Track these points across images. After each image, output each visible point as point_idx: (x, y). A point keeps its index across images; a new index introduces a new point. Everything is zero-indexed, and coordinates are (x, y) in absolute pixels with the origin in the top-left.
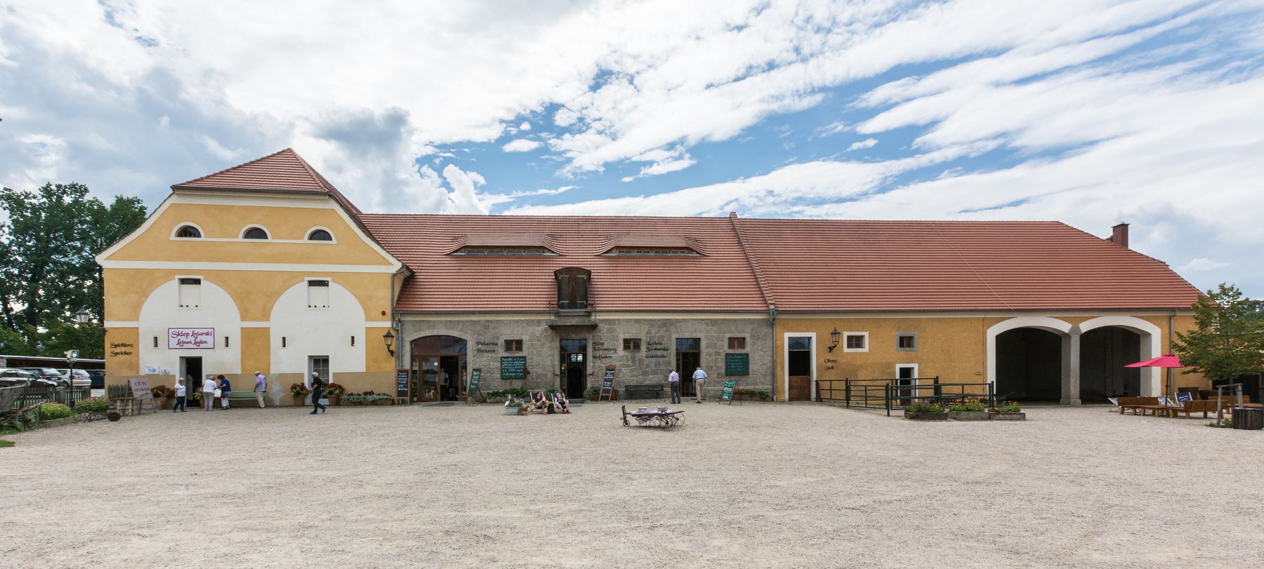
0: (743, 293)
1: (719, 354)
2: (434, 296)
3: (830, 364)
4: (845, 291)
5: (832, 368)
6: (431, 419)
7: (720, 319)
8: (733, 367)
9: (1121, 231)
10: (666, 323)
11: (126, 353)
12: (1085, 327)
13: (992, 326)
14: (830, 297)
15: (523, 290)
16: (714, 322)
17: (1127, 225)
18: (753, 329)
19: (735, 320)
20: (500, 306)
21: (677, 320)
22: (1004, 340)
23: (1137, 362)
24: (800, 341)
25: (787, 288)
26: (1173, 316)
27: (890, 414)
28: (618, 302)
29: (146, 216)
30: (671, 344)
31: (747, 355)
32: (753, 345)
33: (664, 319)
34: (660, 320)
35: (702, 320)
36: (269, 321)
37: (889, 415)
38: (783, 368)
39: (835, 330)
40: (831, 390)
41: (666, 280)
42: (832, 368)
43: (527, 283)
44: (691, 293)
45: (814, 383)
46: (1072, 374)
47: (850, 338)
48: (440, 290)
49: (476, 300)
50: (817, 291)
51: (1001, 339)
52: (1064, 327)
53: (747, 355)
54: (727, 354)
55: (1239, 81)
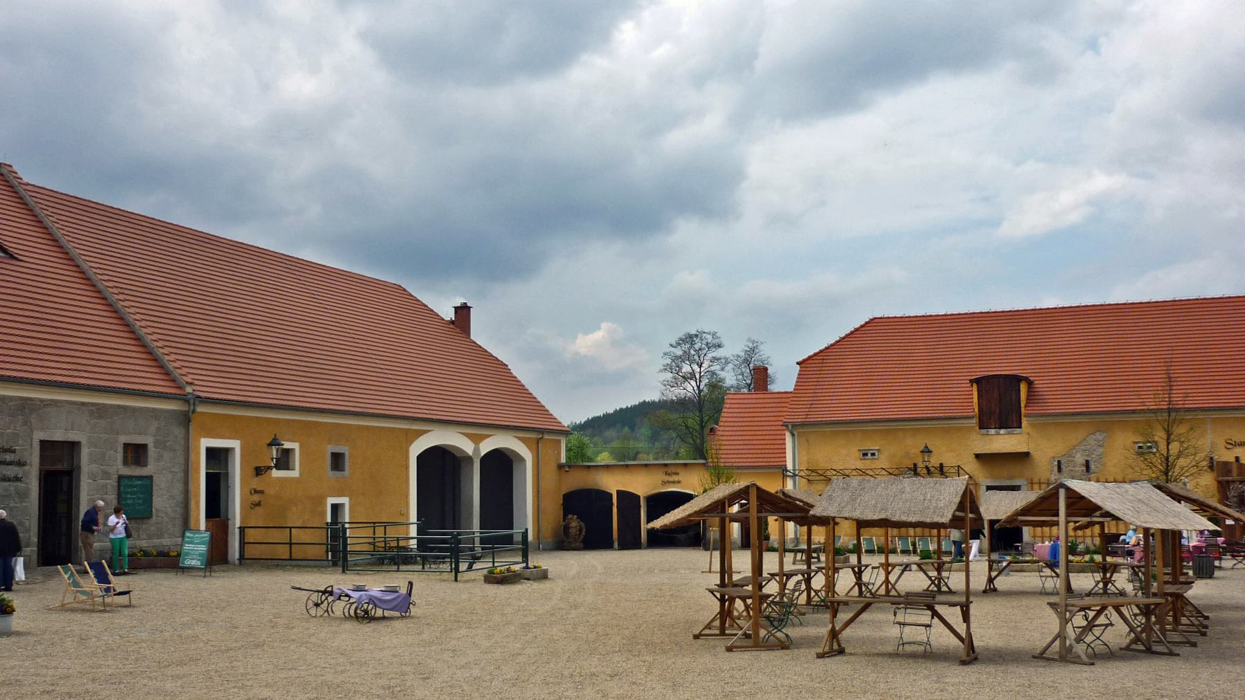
1: (106, 475)
3: (256, 498)
5: (258, 504)
7: (111, 406)
8: (129, 502)
9: (798, 363)
10: (26, 405)
11: (17, 479)
12: (486, 447)
13: (414, 441)
16: (101, 410)
17: (470, 307)
18: (158, 429)
19: (134, 410)
20: (951, 390)
21: (42, 401)
22: (145, 465)
23: (612, 497)
24: (507, 453)
26: (541, 438)
27: (459, 579)
28: (887, 396)
30: (31, 454)
31: (150, 478)
32: (159, 458)
33: (21, 398)
34: (12, 398)
35: (83, 404)
37: (456, 580)
38: (198, 502)
39: (275, 439)
40: (291, 544)
42: (258, 504)
44: (345, 361)
45: (237, 531)
46: (475, 513)
47: (227, 452)
49: (905, 369)
51: (421, 458)
52: (467, 447)
53: (150, 478)
54: (120, 478)
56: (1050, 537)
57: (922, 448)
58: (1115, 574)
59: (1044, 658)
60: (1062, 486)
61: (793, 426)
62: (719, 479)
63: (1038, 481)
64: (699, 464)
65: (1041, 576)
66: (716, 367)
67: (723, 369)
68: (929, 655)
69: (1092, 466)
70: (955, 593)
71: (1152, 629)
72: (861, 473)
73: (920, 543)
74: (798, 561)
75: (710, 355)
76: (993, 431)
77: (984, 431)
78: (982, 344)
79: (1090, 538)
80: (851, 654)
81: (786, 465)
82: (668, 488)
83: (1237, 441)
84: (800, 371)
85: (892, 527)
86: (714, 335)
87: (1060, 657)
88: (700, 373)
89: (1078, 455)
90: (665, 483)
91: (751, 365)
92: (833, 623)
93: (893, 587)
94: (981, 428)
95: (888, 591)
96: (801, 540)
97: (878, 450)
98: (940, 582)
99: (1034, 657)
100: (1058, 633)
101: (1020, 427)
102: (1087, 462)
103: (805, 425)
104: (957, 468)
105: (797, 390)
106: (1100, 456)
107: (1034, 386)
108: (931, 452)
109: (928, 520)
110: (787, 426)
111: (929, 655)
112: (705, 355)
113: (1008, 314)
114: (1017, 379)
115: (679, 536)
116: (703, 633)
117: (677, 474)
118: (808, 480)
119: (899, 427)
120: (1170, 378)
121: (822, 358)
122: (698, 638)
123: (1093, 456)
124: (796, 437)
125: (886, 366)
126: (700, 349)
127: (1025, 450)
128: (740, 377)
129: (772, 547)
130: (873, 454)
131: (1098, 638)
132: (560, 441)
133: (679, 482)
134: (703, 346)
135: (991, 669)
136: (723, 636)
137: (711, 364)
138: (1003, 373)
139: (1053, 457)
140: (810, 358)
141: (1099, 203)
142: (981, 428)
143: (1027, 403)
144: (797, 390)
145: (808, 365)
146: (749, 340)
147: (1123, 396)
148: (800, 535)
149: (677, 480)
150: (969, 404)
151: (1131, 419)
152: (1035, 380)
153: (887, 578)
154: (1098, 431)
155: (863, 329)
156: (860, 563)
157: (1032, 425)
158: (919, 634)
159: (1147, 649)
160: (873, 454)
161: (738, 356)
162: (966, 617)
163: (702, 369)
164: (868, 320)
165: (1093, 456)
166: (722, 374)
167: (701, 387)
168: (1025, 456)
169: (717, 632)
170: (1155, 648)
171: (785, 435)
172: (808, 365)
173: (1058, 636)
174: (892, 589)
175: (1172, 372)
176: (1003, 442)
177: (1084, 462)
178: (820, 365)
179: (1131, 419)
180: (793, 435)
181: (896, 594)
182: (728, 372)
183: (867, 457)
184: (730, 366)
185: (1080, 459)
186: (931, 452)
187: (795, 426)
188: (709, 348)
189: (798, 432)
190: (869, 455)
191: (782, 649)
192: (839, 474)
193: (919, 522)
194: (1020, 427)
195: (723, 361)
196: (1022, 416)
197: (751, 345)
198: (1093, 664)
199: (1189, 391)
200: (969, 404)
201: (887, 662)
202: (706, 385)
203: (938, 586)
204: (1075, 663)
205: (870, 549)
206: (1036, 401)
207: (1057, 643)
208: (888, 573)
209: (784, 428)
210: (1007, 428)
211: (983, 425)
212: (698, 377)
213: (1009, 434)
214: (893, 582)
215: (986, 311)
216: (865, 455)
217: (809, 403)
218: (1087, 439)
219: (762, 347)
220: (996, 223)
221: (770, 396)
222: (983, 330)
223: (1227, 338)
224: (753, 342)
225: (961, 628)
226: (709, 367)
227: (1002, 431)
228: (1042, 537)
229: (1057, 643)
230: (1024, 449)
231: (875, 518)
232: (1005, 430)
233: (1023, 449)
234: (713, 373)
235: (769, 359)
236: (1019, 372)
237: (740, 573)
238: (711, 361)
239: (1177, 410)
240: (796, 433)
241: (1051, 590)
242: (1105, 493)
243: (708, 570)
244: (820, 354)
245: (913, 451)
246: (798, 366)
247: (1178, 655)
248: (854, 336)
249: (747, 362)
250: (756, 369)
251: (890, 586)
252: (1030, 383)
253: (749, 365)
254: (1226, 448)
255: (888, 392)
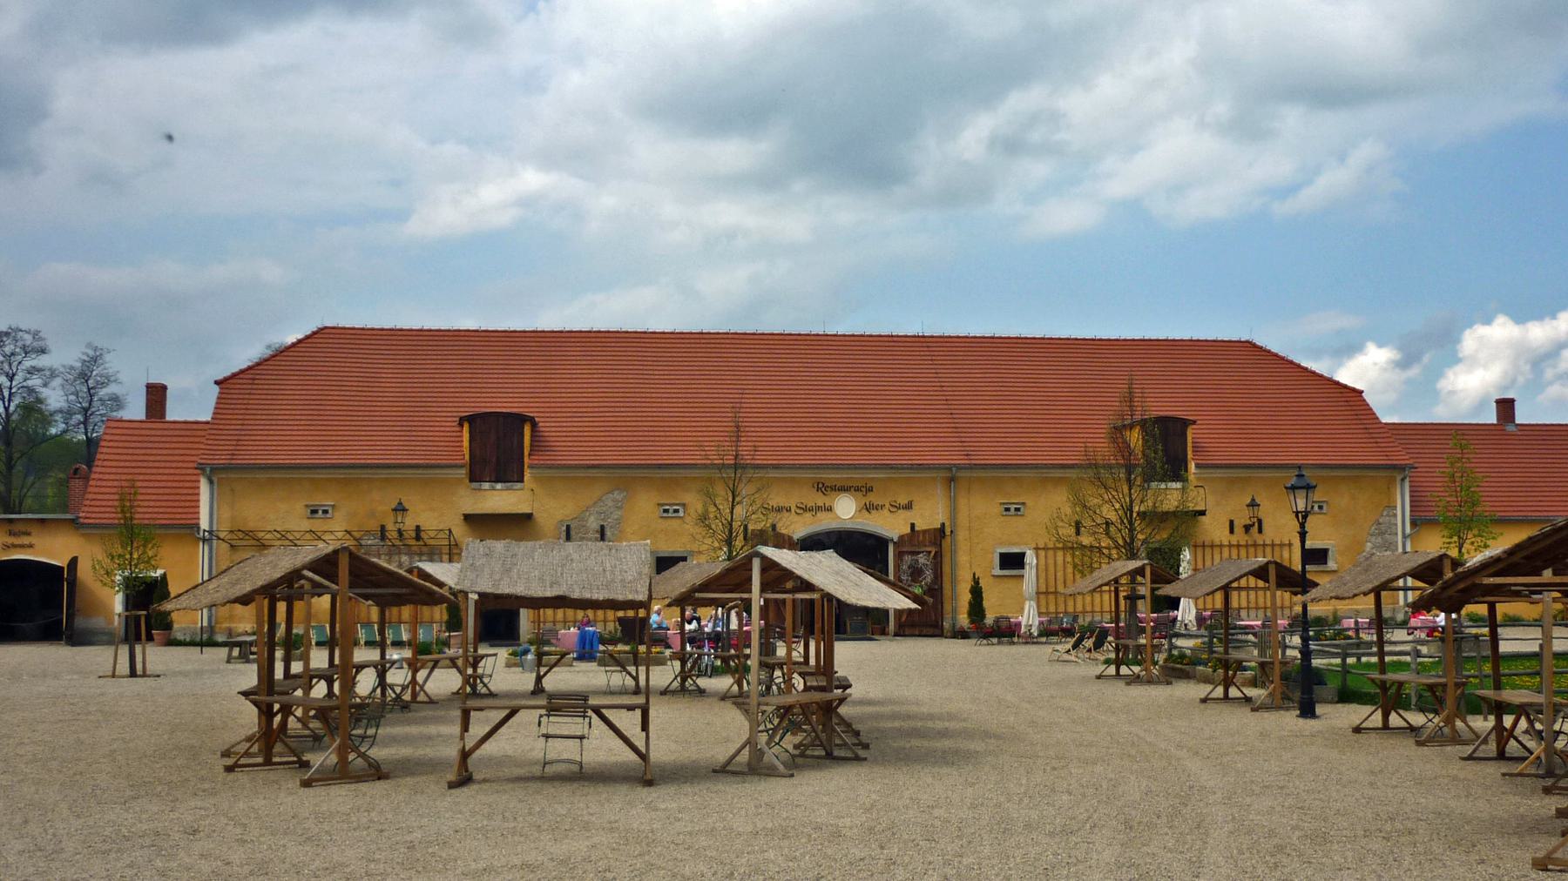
0: (956, 380)
2: (1219, 454)
4: (333, 413)
6: (461, 571)
9: (217, 383)
14: (884, 402)
15: (258, 438)
25: (294, 412)
29: (1401, 712)
36: (657, 558)
39: (400, 504)
41: (391, 357)
43: (574, 367)
48: (768, 373)
50: (161, 445)
55: (951, 717)
56: (575, 622)
57: (1248, 501)
58: (436, 670)
59: (728, 772)
60: (758, 554)
61: (212, 470)
62: (132, 541)
63: (1271, 543)
64: (65, 520)
65: (606, 671)
66: (35, 382)
67: (45, 385)
68: (583, 776)
69: (608, 533)
70: (496, 695)
71: (834, 731)
72: (279, 536)
73: (390, 631)
74: (235, 658)
75: (28, 363)
76: (486, 485)
77: (475, 485)
78: (528, 376)
79: (602, 623)
80: (485, 781)
81: (199, 524)
82: (13, 555)
83: (775, 506)
84: (220, 393)
85: (545, 607)
86: (36, 335)
87: (749, 770)
88: (11, 388)
89: (592, 518)
90: (7, 547)
91: (90, 382)
92: (462, 738)
93: (422, 688)
94: (472, 480)
95: (414, 695)
96: (217, 630)
97: (333, 506)
98: (475, 681)
99: (715, 771)
100: (748, 739)
101: (522, 481)
102: (602, 527)
103: (231, 468)
104: (447, 532)
105: (216, 419)
106: (619, 521)
107: (538, 429)
108: (407, 510)
109: (620, 598)
110: (203, 469)
111: (583, 776)
112: (20, 363)
113: (578, 335)
114: (519, 420)
115: (24, 625)
116: (239, 763)
117: (29, 534)
118: (232, 546)
119: (363, 476)
120: (737, 427)
121: (251, 376)
122: (233, 771)
123: (609, 520)
124: (215, 487)
125: (975, 398)
126: (13, 354)
127: (528, 510)
128: (72, 397)
129: (176, 639)
130: (325, 512)
131: (1431, 720)
132: (1395, 477)
133: (31, 546)
134: (18, 350)
135: (671, 789)
136: (269, 765)
137: (28, 376)
138: (504, 410)
139: (562, 521)
140: (234, 376)
141: (527, 202)
142: (472, 480)
143: (531, 450)
144: (216, 419)
145: (232, 386)
146: (89, 345)
147: (913, 442)
148: (216, 623)
149: (27, 543)
150: (458, 449)
151: (658, 476)
152: (539, 422)
153: (414, 677)
154: (618, 489)
155: (310, 340)
156: (385, 658)
157: (535, 479)
158: (568, 750)
159: (827, 754)
160: (325, 512)
161: (72, 368)
162: (645, 726)
163: (14, 383)
164: (315, 329)
165: (609, 520)
166: (45, 393)
167: (12, 408)
168: (528, 517)
169: (260, 760)
170: (836, 753)
171: (199, 481)
172: (232, 386)
173: (748, 742)
174: (420, 691)
175: (741, 420)
176: (499, 499)
177: (599, 528)
178: (250, 386)
179: (658, 476)
180: (211, 482)
181: (426, 699)
182: (54, 389)
183: (317, 516)
184: (57, 382)
185: (593, 523)
186: (407, 510)
187: (215, 469)
188: (26, 353)
189: (218, 479)
190: (320, 512)
191: (379, 779)
192: (247, 537)
193: (608, 600)
194: (522, 481)
195: (48, 373)
196: (526, 467)
197: (91, 353)
198: (792, 776)
199: (1098, 445)
200: (458, 449)
201: (533, 786)
202: (18, 406)
203: (474, 687)
204: (769, 775)
205: (371, 639)
206: (543, 449)
207: (746, 751)
208: (415, 672)
209: (199, 471)
210: (505, 482)
211: (475, 477)
212: (6, 394)
213: (508, 489)
214: (421, 682)
215: (752, 332)
216: (314, 512)
217: (236, 438)
218: (604, 498)
219: (107, 357)
220: (402, 216)
221: (166, 426)
222: (470, 353)
223: (667, 382)
224: (96, 349)
225: (639, 741)
226: (25, 380)
227: (499, 486)
228: (565, 622)
229: (746, 751)
230: (525, 509)
231: (548, 594)
232: (503, 484)
233: (524, 509)
234: (31, 390)
235: (118, 375)
236: (1185, 413)
237: (158, 676)
238: (29, 373)
239: (745, 467)
240: (215, 479)
241: (617, 689)
242: (803, 563)
243: (110, 673)
244: (241, 376)
245: (380, 508)
246: (216, 386)
247: (865, 759)
248: (297, 349)
249: (84, 376)
250: (151, 387)
251: (418, 688)
252: (534, 425)
253: (87, 381)
254: (796, 513)
255: (927, 425)
